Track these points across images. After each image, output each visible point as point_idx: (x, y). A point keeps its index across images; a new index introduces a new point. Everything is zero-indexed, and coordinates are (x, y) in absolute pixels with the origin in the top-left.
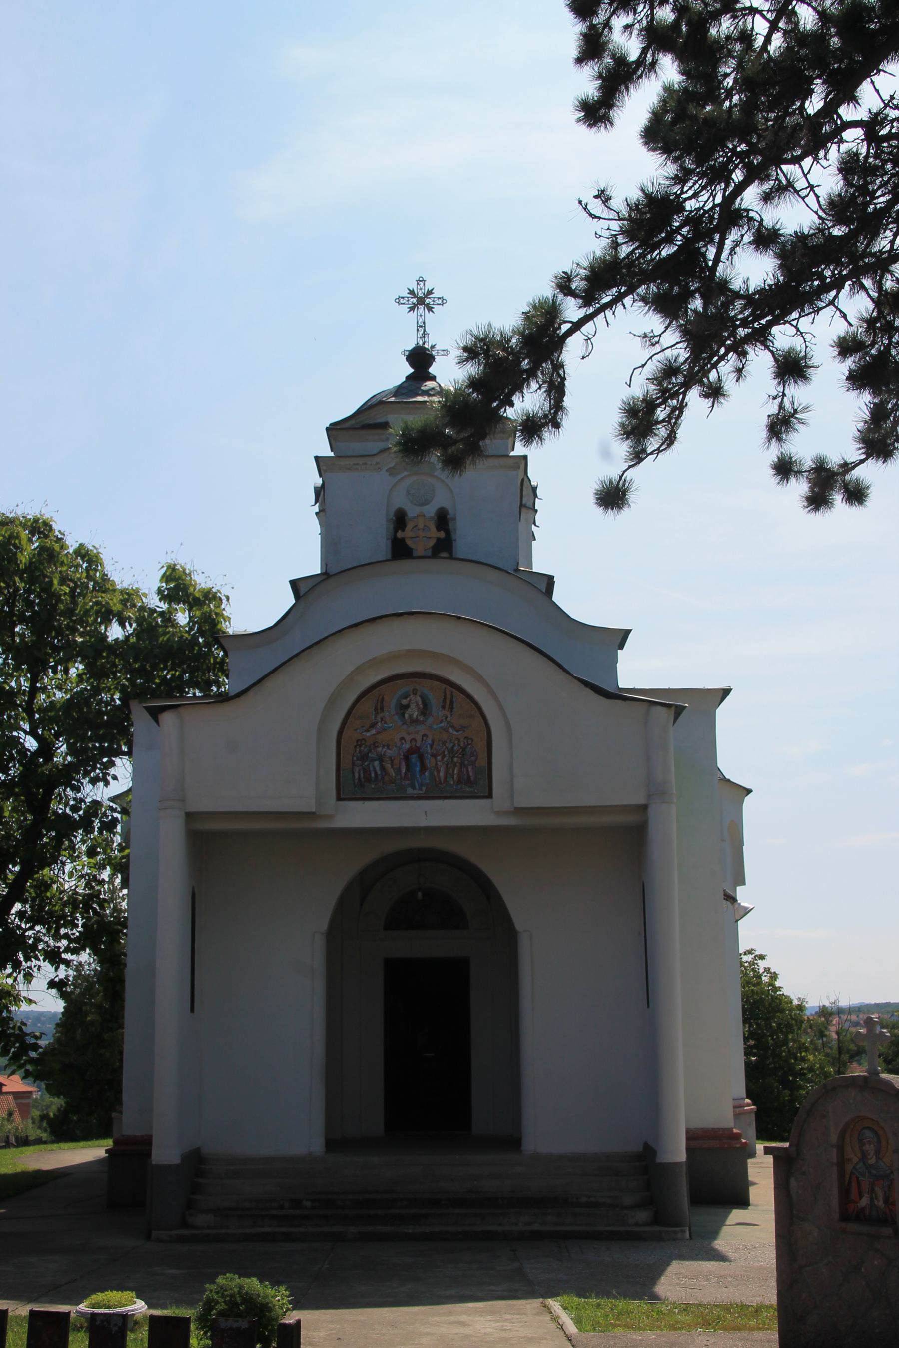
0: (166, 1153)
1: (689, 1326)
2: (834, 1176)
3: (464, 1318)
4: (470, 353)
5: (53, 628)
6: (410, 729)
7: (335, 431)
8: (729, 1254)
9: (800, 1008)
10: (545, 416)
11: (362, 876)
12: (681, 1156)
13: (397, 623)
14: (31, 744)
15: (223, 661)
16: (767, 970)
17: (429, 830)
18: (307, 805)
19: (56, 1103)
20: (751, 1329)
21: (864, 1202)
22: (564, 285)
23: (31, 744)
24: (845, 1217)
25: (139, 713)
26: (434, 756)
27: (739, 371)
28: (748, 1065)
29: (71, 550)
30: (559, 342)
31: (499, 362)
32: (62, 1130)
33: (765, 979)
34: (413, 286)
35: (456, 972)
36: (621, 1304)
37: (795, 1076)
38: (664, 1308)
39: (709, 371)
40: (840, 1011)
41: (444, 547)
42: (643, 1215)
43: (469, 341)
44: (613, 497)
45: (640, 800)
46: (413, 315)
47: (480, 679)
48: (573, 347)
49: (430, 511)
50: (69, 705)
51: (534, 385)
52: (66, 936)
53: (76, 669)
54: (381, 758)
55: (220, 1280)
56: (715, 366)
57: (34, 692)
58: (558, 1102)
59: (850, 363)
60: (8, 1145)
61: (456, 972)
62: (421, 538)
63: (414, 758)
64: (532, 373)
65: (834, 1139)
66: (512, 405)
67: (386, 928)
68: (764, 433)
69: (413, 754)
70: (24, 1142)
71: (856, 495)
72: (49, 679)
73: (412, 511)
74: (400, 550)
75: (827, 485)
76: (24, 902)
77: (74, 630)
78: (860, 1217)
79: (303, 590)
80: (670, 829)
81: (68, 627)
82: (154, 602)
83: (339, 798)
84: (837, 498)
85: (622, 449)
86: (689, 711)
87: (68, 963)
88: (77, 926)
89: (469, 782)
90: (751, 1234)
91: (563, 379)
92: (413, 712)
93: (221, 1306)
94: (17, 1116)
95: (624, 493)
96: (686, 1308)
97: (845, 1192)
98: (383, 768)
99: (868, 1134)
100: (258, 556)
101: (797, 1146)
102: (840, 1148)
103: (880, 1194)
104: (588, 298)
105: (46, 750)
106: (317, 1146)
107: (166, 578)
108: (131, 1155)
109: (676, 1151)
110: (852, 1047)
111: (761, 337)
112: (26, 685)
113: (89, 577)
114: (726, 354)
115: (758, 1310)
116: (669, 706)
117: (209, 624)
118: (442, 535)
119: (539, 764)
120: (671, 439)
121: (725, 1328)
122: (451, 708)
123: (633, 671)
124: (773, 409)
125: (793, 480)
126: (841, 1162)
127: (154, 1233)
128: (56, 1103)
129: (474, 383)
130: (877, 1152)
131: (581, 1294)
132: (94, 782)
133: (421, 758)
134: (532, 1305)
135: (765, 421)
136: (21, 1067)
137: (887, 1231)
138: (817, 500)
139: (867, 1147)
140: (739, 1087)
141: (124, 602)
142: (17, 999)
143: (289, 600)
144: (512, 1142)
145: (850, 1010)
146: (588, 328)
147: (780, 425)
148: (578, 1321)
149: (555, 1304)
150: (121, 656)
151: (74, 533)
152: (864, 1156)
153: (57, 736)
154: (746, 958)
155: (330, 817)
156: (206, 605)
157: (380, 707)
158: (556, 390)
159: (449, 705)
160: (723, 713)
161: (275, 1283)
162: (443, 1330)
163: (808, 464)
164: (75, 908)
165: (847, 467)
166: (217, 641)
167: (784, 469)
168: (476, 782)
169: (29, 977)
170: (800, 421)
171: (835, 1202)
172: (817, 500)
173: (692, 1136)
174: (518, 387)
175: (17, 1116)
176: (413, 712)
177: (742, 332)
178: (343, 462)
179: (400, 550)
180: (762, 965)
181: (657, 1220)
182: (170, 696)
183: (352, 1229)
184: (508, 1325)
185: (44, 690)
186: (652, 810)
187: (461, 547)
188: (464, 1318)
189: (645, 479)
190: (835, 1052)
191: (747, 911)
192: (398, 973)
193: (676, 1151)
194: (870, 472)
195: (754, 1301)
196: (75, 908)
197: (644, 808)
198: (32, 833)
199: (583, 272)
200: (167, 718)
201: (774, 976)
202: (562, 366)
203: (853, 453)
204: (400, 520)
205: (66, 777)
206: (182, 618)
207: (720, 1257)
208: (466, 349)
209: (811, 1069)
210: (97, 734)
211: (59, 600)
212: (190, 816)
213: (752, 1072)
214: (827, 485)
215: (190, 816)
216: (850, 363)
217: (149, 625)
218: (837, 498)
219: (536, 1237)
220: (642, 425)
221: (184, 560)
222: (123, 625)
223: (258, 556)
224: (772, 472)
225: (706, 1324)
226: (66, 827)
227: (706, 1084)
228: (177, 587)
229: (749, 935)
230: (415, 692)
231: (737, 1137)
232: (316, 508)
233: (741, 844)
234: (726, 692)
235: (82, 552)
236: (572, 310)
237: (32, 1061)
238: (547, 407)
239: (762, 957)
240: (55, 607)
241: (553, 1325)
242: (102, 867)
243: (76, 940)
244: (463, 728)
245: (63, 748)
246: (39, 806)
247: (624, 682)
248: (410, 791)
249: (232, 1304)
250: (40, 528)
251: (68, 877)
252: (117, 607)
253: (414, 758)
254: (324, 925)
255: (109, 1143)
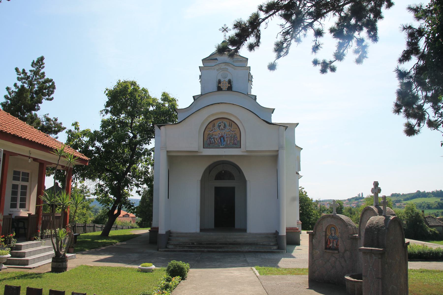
0: (162, 231)
1: (286, 274)
2: (324, 238)
3: (232, 271)
4: (236, 26)
5: (136, 107)
6: (222, 131)
7: (204, 60)
8: (296, 257)
9: (312, 200)
10: (255, 43)
11: (209, 166)
12: (285, 234)
13: (218, 105)
14: (131, 135)
15: (176, 116)
16: (305, 191)
17: (226, 156)
18: (196, 150)
19: (139, 219)
20: (301, 274)
21: (331, 245)
22: (261, 8)
23: (131, 135)
24: (326, 248)
25: (156, 127)
26: (227, 138)
27: (305, 35)
28: (300, 213)
29: (141, 89)
30: (259, 24)
31: (243, 28)
32: (141, 225)
33: (304, 193)
34: (223, 26)
35: (232, 189)
36: (270, 268)
37: (310, 216)
38: (280, 269)
39: (297, 34)
40: (320, 201)
41: (230, 89)
42: (275, 247)
43: (236, 23)
44: (272, 67)
45: (277, 149)
46: (223, 33)
47: (238, 119)
48: (263, 25)
49: (227, 80)
50: (140, 126)
51: (252, 35)
52: (140, 181)
53: (142, 117)
54: (214, 138)
55: (172, 262)
56: (299, 33)
57: (132, 123)
58: (256, 222)
59: (333, 34)
60: (129, 228)
61: (232, 189)
62: (225, 86)
63: (222, 138)
64: (252, 32)
65: (324, 230)
66: (246, 41)
67: (215, 179)
68: (311, 50)
69: (222, 138)
70: (132, 228)
71: (333, 70)
72: (136, 120)
73: (222, 80)
74: (219, 89)
75: (326, 67)
76: (130, 172)
77: (141, 108)
78: (330, 248)
79: (196, 98)
80: (284, 157)
81: (140, 107)
82: (160, 101)
83: (204, 148)
84: (328, 70)
85: (275, 54)
86: (288, 128)
87: (140, 187)
88: (142, 178)
89: (235, 144)
90: (302, 252)
91: (260, 34)
92: (222, 127)
93: (172, 268)
94: (132, 222)
95: (275, 66)
96: (286, 269)
97: (326, 243)
98: (214, 140)
99: (333, 228)
100: (185, 89)
101: (315, 232)
102: (326, 232)
103: (335, 243)
104: (267, 12)
105: (135, 137)
106: (198, 230)
107: (163, 95)
108: (154, 231)
109: (283, 233)
110: (323, 209)
111: (311, 24)
112: (130, 121)
113: (145, 96)
114: (301, 30)
115: (303, 270)
116: (284, 126)
117: (173, 107)
118: (229, 85)
119: (253, 140)
120: (287, 53)
121: (295, 274)
122: (231, 126)
123: (275, 119)
124: (314, 44)
125: (317, 65)
126: (326, 235)
127: (159, 249)
128: (139, 219)
129: (237, 35)
130: (335, 233)
131: (261, 266)
132: (146, 144)
133: (224, 138)
134: (249, 268)
135: (311, 47)
136: (130, 211)
137: (336, 252)
138: (323, 71)
139: (332, 232)
140: (298, 218)
141: (153, 101)
142: (129, 195)
143: (193, 100)
144: (244, 230)
145: (323, 201)
146: (266, 20)
147: (316, 48)
148: (259, 273)
149: (254, 268)
150: (152, 114)
151: (141, 85)
152: (331, 234)
153: (137, 133)
154: (300, 189)
155: (202, 152)
156: (172, 102)
157: (214, 126)
158: (258, 37)
159: (230, 126)
160: (297, 129)
161: (186, 262)
162: (226, 274)
163: (321, 61)
164: (142, 174)
165: (331, 62)
166: (175, 110)
167: (315, 62)
168: (237, 144)
169: (131, 190)
170: (321, 47)
171: (324, 245)
172: (323, 71)
173: (287, 229)
174: (248, 36)
175: (132, 222)
176: (222, 127)
177: (306, 24)
178: (206, 68)
179: (219, 89)
180: (303, 190)
181: (279, 248)
182: (164, 123)
183: (206, 250)
184: (242, 273)
185: (134, 122)
186: (279, 151)
187: (234, 89)
188: (232, 271)
189: (280, 62)
190: (319, 210)
191: (301, 177)
192: (218, 190)
193: (283, 233)
194: (336, 64)
195: (302, 267)
196: (142, 174)
197: (278, 151)
198: (132, 156)
199: (265, 6)
200: (162, 128)
201: (306, 193)
202: (260, 31)
203: (333, 59)
204: (219, 82)
205: (139, 143)
206: (167, 105)
207: (294, 257)
208: (234, 25)
209: (314, 214)
210: (148, 133)
211: (138, 101)
212: (167, 151)
213: (301, 215)
214: (326, 67)
215: (167, 151)
216: (333, 34)
217: (159, 106)
218: (328, 70)
219: (250, 252)
220: (280, 48)
221: (167, 91)
222: (153, 107)
223: (185, 89)
224: (312, 63)
225: (291, 273)
226: (139, 155)
227: (291, 217)
228: (165, 97)
229: (302, 183)
230: (222, 122)
231: (298, 229)
232: (200, 80)
233: (300, 161)
234: (298, 124)
235: (144, 90)
236: (262, 15)
237: (132, 209)
238: (255, 41)
239: (303, 188)
240: (137, 102)
241: (253, 273)
242: (148, 165)
243: (143, 182)
244: (234, 131)
245: (138, 137)
246: (133, 150)
247: (273, 121)
248: (221, 146)
249: (175, 267)
250: (133, 84)
251: (140, 167)
252: (151, 102)
253: (222, 138)
254: (200, 178)
255: (150, 229)
